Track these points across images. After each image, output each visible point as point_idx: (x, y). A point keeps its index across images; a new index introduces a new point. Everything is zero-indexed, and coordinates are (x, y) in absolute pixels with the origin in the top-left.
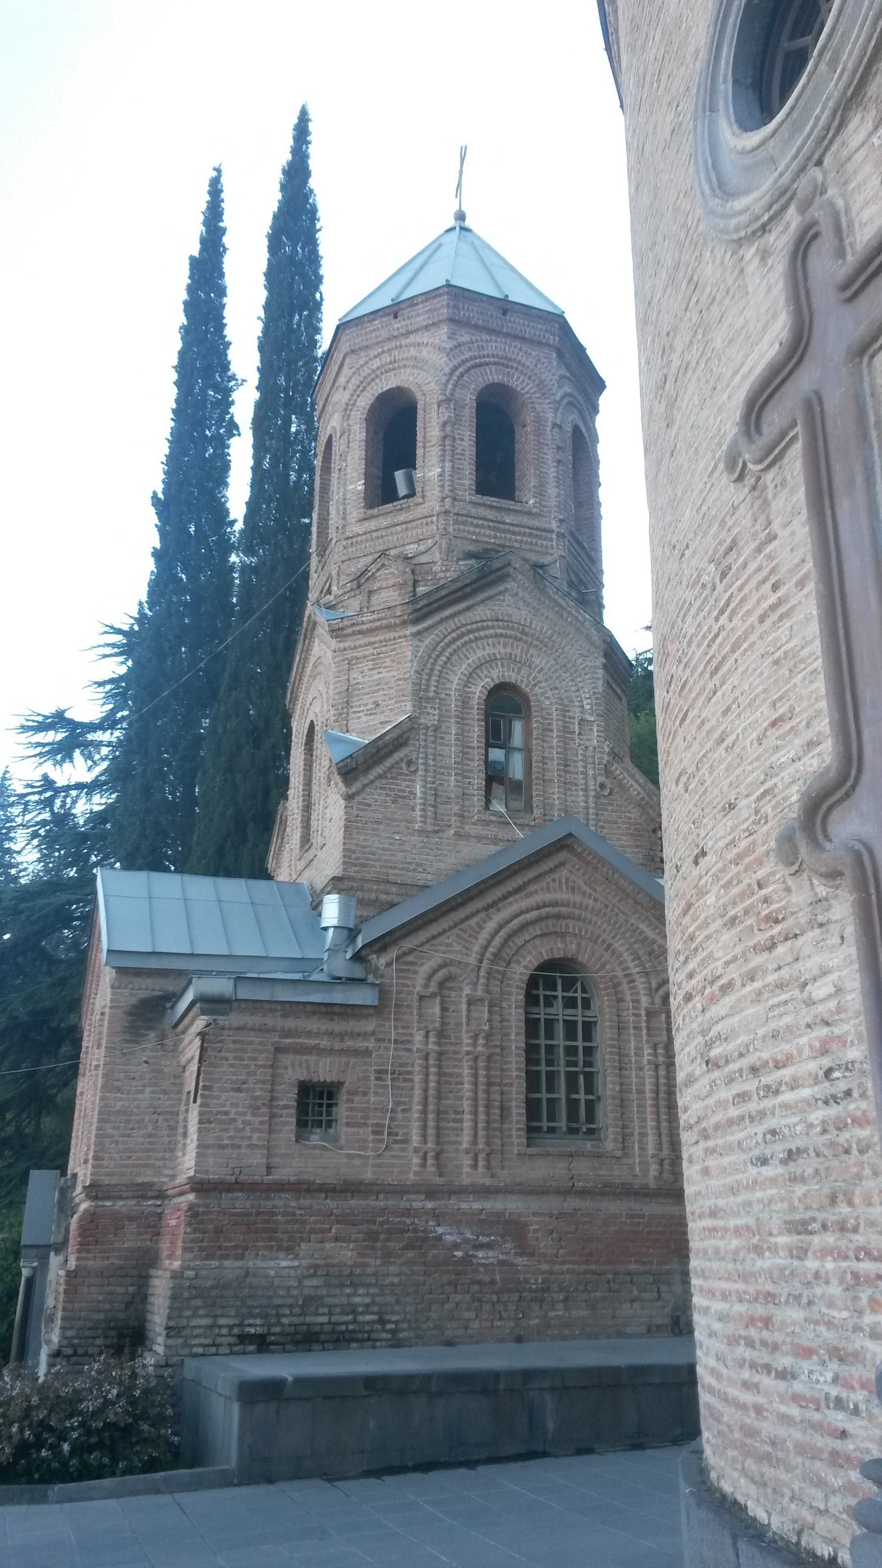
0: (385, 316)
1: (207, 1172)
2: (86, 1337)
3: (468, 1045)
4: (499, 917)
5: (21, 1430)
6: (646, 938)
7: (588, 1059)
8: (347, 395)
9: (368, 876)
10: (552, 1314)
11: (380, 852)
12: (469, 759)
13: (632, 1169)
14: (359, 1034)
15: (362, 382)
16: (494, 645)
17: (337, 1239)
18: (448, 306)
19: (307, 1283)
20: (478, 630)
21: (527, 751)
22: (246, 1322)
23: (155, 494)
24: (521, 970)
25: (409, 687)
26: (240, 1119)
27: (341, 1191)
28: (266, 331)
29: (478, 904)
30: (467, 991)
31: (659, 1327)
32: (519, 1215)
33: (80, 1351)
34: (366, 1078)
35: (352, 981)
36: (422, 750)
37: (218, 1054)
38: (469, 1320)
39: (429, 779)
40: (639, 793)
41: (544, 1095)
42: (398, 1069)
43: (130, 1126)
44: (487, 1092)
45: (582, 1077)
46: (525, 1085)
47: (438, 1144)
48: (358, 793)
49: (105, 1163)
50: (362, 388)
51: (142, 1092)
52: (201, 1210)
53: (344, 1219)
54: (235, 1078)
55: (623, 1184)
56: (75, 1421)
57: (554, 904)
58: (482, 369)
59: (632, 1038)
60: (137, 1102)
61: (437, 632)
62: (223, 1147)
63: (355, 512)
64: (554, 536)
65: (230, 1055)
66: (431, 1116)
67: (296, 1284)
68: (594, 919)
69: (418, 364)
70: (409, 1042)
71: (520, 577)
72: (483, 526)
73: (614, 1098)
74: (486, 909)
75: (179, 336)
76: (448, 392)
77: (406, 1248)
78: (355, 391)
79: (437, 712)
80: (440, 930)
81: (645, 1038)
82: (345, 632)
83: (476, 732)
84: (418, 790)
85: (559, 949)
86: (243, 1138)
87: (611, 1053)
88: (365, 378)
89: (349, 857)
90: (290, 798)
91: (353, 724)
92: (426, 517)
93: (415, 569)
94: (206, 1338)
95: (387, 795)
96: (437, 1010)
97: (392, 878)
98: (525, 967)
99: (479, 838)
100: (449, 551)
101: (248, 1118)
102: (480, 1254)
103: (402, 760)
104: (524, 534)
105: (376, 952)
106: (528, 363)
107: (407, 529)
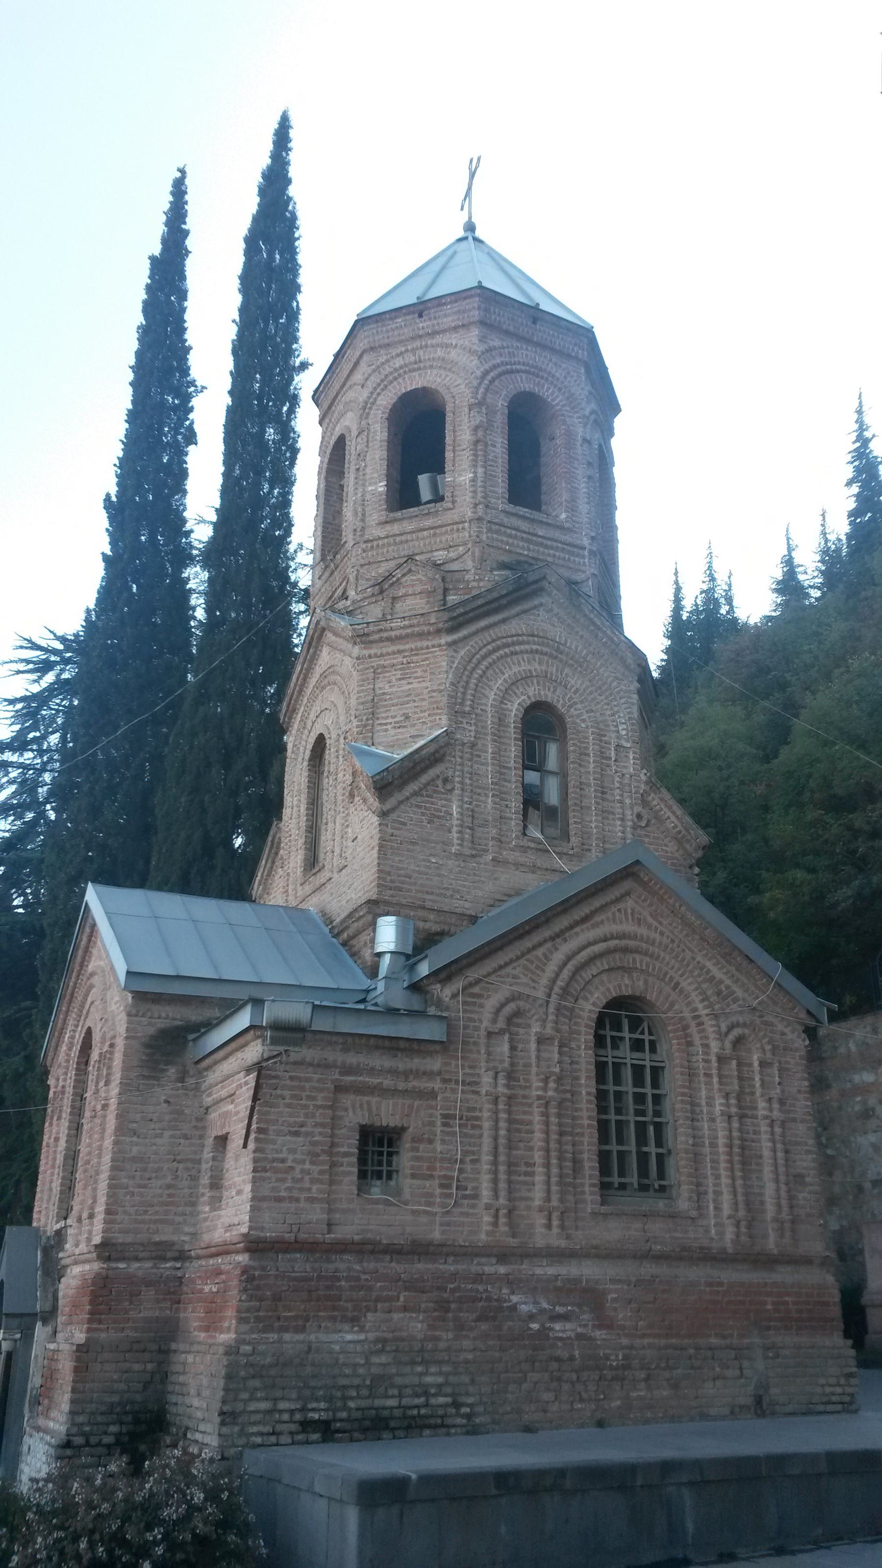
0: (409, 314)
1: (262, 1229)
2: (97, 1424)
3: (538, 1089)
4: (565, 948)
5: (92, 1545)
6: (714, 978)
7: (657, 1108)
8: (365, 393)
9: (404, 901)
10: (634, 1394)
11: (415, 875)
12: (505, 780)
13: (707, 1231)
14: (425, 1073)
15: (382, 381)
16: (529, 661)
17: (405, 1309)
18: (479, 308)
19: (375, 1360)
20: (513, 644)
21: (563, 775)
22: (310, 1406)
23: (108, 496)
24: (589, 1007)
25: (445, 699)
26: (298, 1168)
27: (408, 1253)
28: (241, 334)
29: (546, 933)
30: (536, 1028)
31: (741, 1407)
32: (597, 1282)
33: (93, 1440)
34: (432, 1124)
35: (411, 1013)
36: (458, 767)
37: (274, 1092)
38: (547, 1402)
39: (466, 799)
40: (676, 826)
41: (614, 1147)
42: (465, 1114)
43: (147, 1175)
44: (559, 1142)
45: (651, 1128)
46: (597, 1135)
47: (510, 1200)
48: (393, 810)
49: (119, 1217)
50: (383, 385)
51: (160, 1136)
52: (257, 1273)
53: (412, 1286)
54: (292, 1120)
55: (701, 1248)
56: (158, 1533)
57: (622, 936)
58: (513, 376)
59: (703, 1086)
60: (154, 1148)
61: (472, 643)
62: (279, 1200)
63: (376, 514)
64: (586, 553)
65: (287, 1093)
66: (502, 1168)
67: (363, 1362)
68: (662, 954)
69: (446, 365)
70: (477, 1083)
71: (555, 592)
72: (516, 537)
73: (687, 1152)
74: (552, 939)
75: (137, 335)
76: (479, 396)
77: (478, 1319)
78: (375, 389)
79: (473, 728)
80: (507, 959)
81: (716, 1086)
82: (371, 638)
83: (513, 751)
84: (455, 810)
85: (626, 986)
86: (301, 1190)
87: (683, 1102)
88: (386, 376)
89: (384, 879)
90: (285, 818)
91: (379, 737)
92: (457, 523)
93: (445, 578)
94: (264, 1425)
95: (423, 814)
96: (506, 1048)
97: (428, 904)
98: (594, 1004)
99: (517, 865)
100: (483, 560)
101: (307, 1166)
102: (557, 1326)
103: (438, 776)
104: (557, 548)
105: (440, 982)
106: (558, 375)
107: (435, 535)
